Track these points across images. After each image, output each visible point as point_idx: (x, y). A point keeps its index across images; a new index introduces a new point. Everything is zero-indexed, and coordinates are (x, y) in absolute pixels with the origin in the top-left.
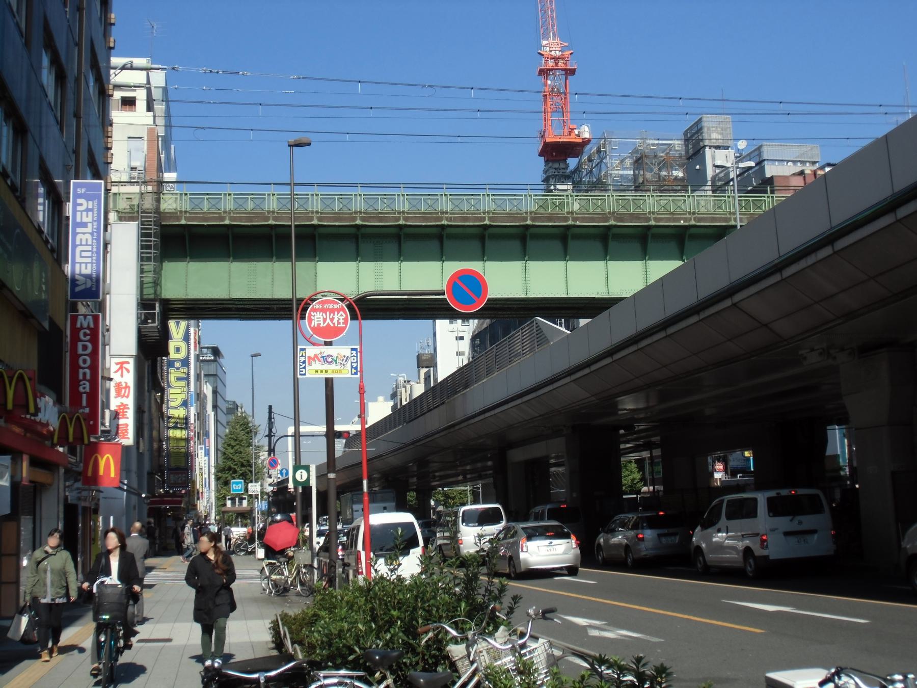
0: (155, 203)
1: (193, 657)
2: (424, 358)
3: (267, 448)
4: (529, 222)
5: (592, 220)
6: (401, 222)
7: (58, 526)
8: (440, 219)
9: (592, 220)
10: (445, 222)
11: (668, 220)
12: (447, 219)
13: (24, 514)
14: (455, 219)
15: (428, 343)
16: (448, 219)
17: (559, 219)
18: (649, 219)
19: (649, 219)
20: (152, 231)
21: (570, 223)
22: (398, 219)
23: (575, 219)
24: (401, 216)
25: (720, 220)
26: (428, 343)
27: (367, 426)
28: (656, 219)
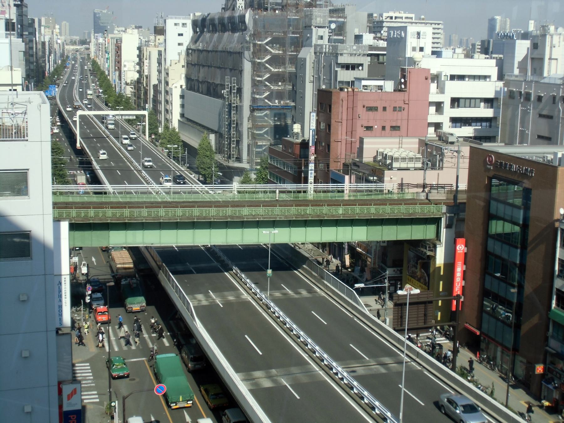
0: (205, 67)
1: (85, 345)
2: (158, 28)
3: (16, 100)
4: (195, 220)
5: (221, 219)
6: (144, 221)
7: (550, 348)
8: (160, 219)
9: (221, 219)
10: (161, 221)
11: (252, 218)
12: (163, 219)
13: (518, 233)
14: (166, 219)
15: (161, 15)
16: (163, 220)
17: (208, 219)
18: (244, 218)
19: (244, 218)
20: (81, 190)
21: (212, 220)
22: (143, 220)
23: (214, 219)
24: (144, 218)
25: (273, 218)
26: (161, 15)
27: (521, 222)
28: (247, 218)
